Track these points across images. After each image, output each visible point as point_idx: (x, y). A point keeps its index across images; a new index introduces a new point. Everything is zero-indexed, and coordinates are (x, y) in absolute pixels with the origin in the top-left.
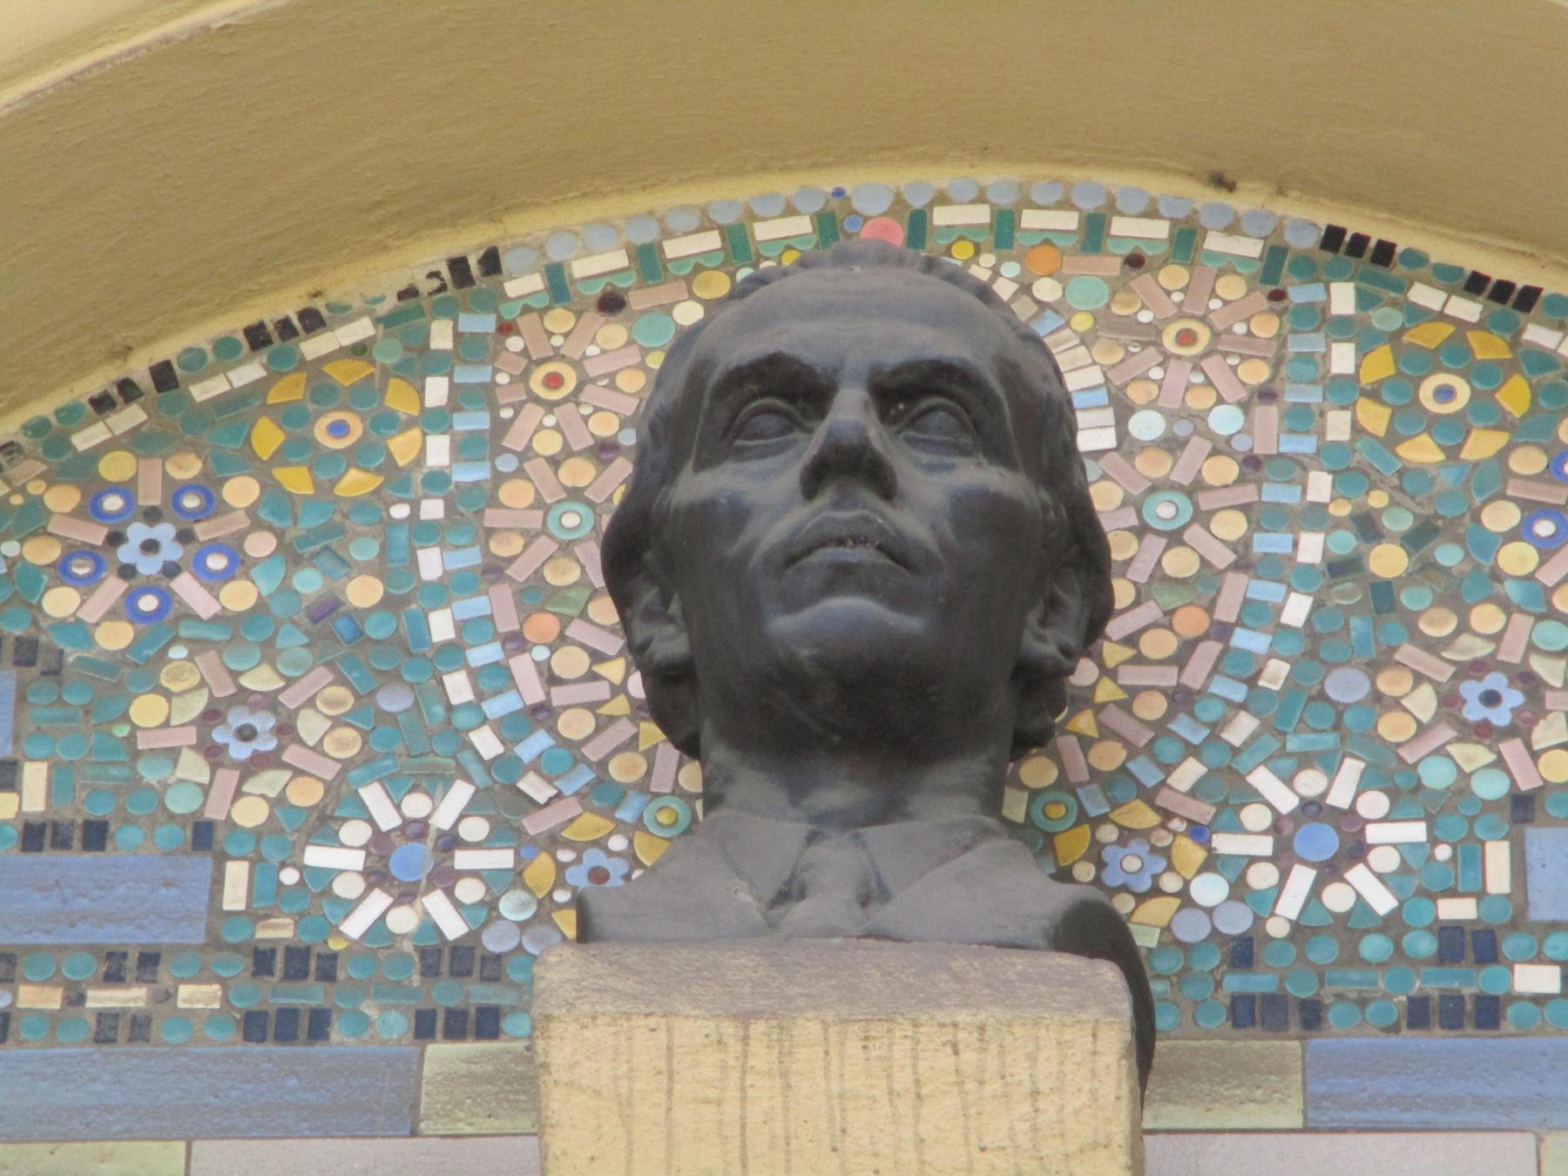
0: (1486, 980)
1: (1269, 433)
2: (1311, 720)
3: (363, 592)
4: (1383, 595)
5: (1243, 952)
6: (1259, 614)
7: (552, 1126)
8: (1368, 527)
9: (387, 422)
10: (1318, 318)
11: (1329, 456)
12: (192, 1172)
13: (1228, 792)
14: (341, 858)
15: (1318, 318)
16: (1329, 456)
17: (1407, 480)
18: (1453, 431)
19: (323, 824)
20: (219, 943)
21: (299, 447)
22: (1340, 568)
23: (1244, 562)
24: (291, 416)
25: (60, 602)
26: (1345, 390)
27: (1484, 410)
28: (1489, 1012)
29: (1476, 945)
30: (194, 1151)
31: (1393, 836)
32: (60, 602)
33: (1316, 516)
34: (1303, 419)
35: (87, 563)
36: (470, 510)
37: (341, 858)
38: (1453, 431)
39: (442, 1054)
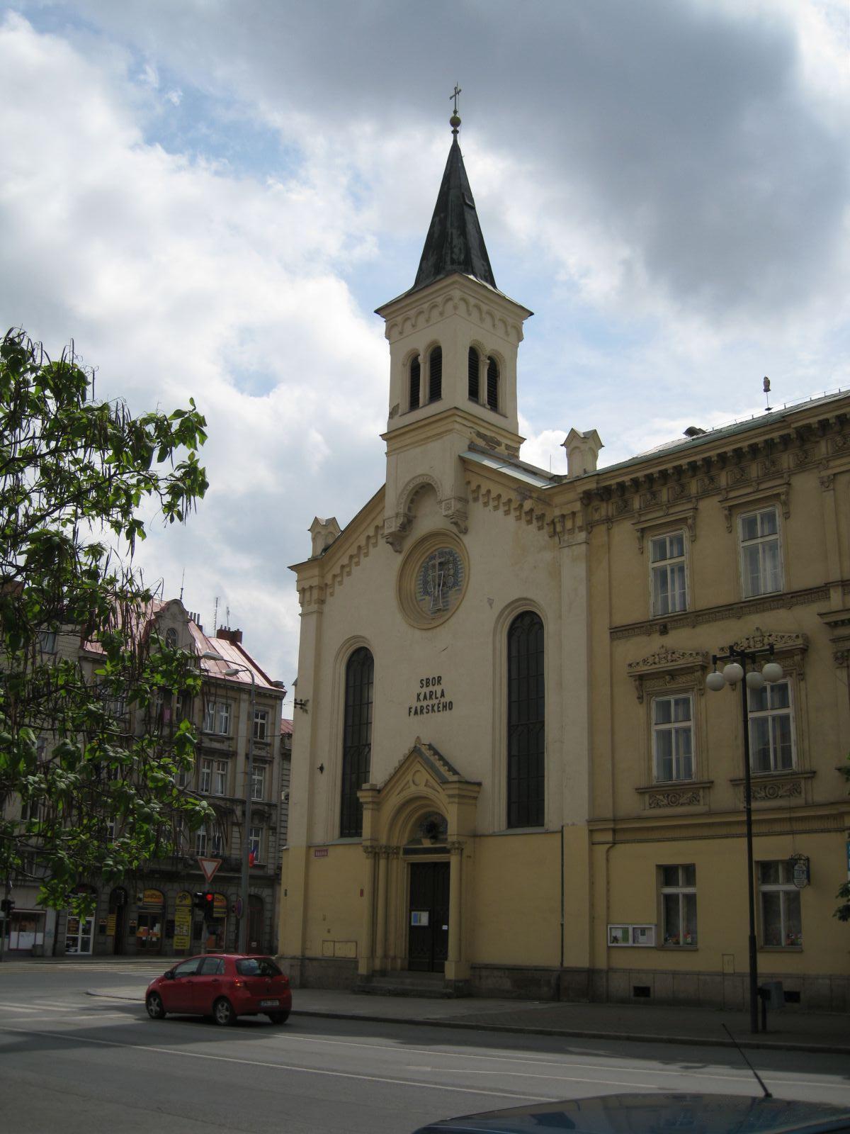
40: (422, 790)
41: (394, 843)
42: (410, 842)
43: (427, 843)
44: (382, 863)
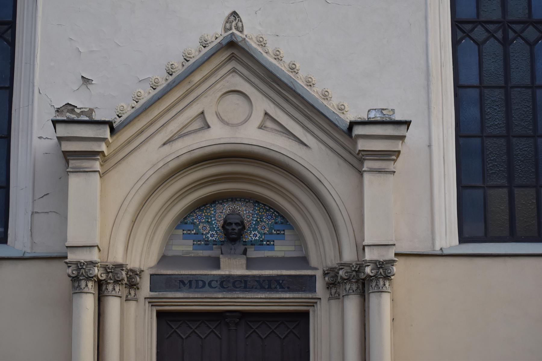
0: (262, 243)
1: (253, 213)
2: (255, 229)
3: (210, 220)
4: (258, 222)
5: (251, 241)
6: (253, 223)
7: (394, 275)
8: (258, 218)
9: (210, 211)
10: (255, 206)
11: (256, 214)
12: (474, 4)
13: (251, 233)
14: (209, 235)
15: (255, 206)
16: (256, 214)
17: (260, 215)
18: (262, 213)
19: (208, 233)
20: (204, 240)
21: (206, 212)
22: (257, 220)
23: (252, 220)
24: (206, 210)
25: (195, 221)
26: (257, 210)
27: (263, 212)
28: (262, 245)
29: (262, 241)
30: (466, 84)
31: (258, 235)
32: (195, 221)
33: (255, 217)
34: (255, 212)
35: (197, 218)
36: (214, 216)
37: (209, 235)
38: (262, 213)
39: (214, 246)
40: (252, 135)
41: (133, 263)
42: (164, 260)
43: (234, 267)
44: (113, 305)
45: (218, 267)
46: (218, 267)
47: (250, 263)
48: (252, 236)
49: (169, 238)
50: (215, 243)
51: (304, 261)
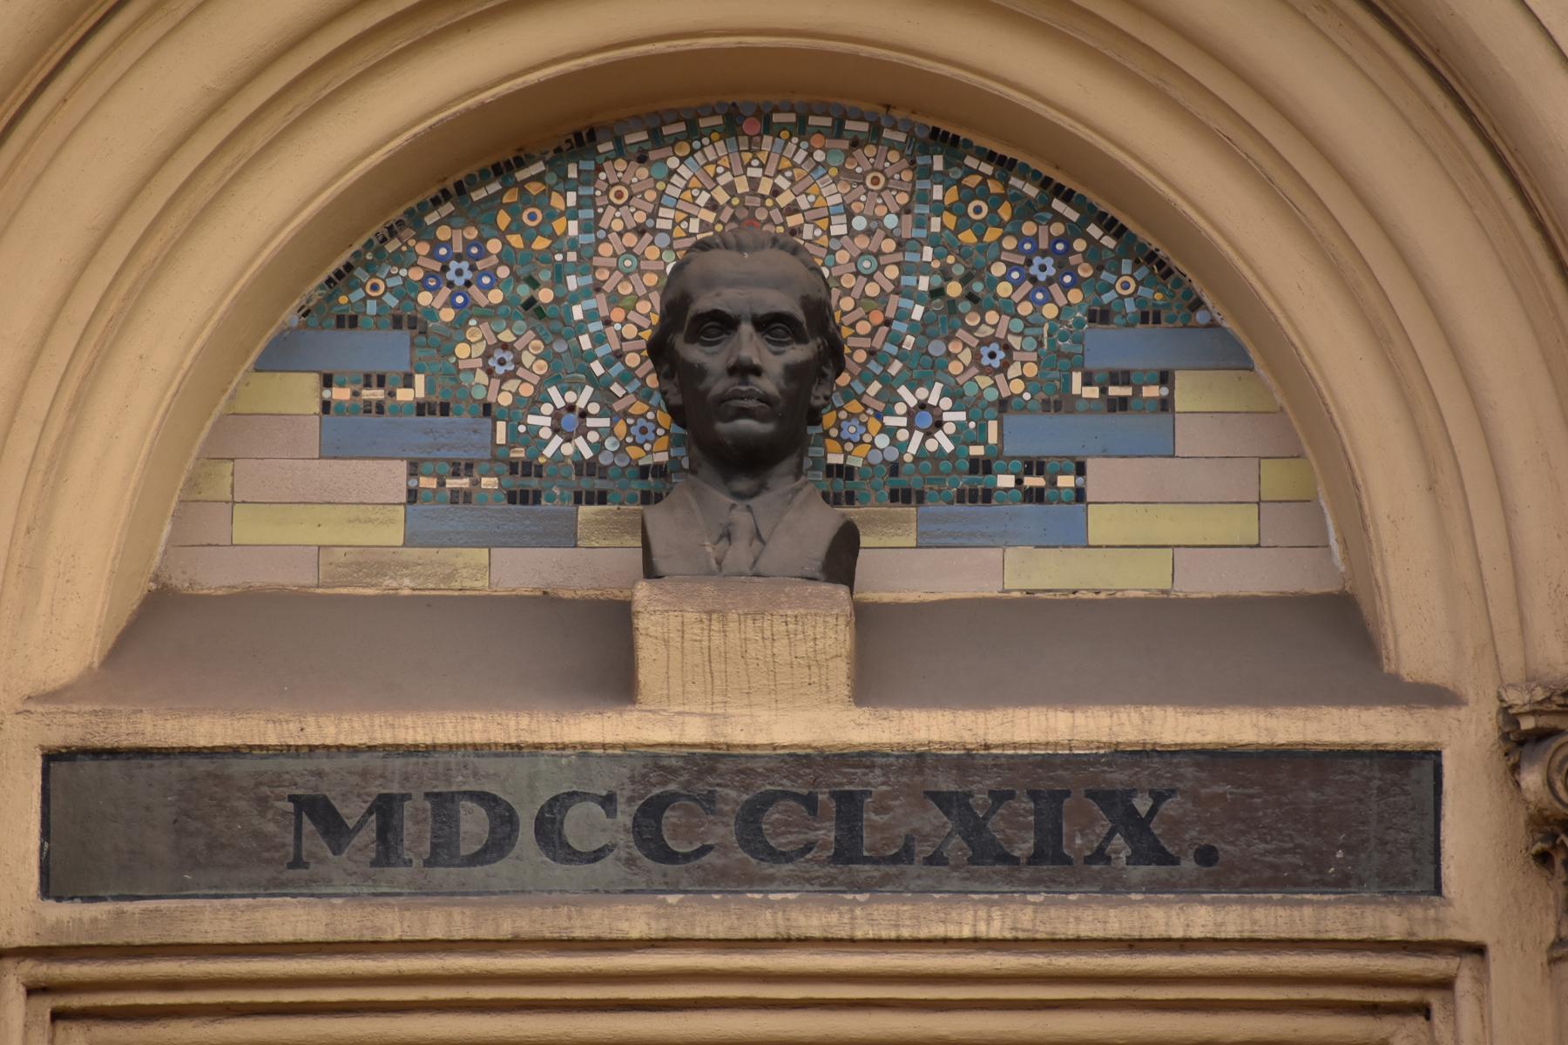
42: (160, 624)
43: (746, 682)
45: (618, 682)
46: (618, 682)
47: (885, 650)
48: (882, 427)
49: (208, 447)
50: (591, 484)
51: (1336, 631)
